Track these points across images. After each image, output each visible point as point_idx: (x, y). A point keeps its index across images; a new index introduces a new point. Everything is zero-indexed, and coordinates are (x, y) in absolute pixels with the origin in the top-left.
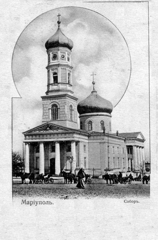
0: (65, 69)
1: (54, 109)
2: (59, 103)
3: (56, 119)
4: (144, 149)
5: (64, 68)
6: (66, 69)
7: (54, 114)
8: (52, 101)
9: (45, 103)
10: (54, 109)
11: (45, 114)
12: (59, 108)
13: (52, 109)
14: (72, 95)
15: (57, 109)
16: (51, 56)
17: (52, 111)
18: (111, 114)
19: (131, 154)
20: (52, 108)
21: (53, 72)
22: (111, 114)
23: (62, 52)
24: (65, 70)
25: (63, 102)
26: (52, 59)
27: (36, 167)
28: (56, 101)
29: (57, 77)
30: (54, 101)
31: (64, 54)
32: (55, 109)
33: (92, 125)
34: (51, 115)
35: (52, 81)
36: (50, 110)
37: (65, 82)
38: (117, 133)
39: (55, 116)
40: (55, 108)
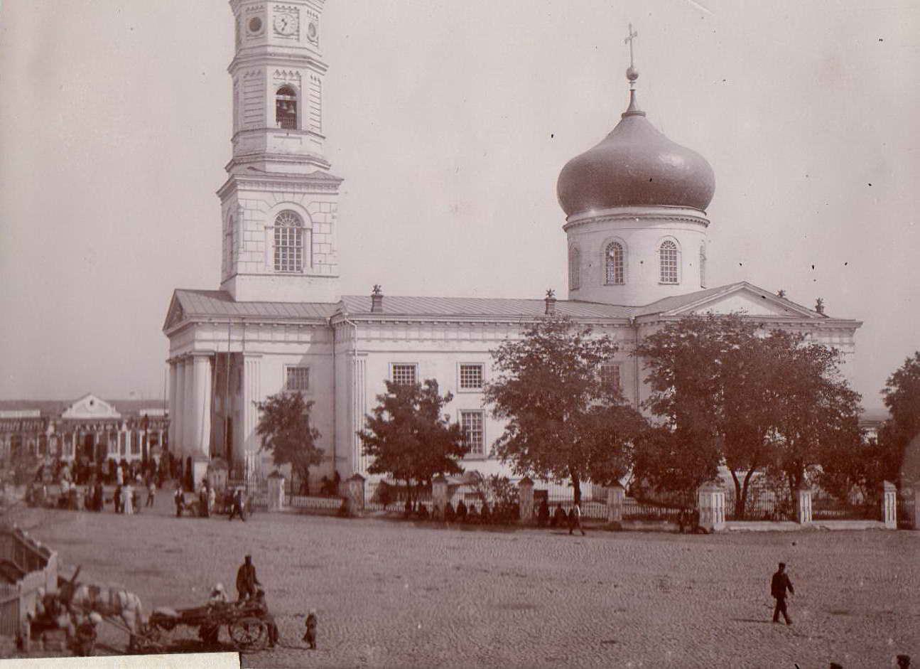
0: (297, 73)
1: (284, 231)
2: (305, 204)
3: (292, 268)
4: (320, 612)
5: (294, 71)
6: (320, 82)
7: (284, 249)
8: (279, 197)
10: (284, 231)
13: (277, 230)
14: (275, 134)
15: (299, 232)
16: (245, 25)
17: (277, 237)
18: (706, 214)
19: (656, 491)
20: (277, 223)
25: (325, 208)
26: (247, 32)
27: (7, 489)
28: (297, 198)
30: (288, 197)
32: (291, 231)
33: (232, 238)
36: (272, 233)
38: (377, 297)
39: (292, 256)
40: (288, 226)
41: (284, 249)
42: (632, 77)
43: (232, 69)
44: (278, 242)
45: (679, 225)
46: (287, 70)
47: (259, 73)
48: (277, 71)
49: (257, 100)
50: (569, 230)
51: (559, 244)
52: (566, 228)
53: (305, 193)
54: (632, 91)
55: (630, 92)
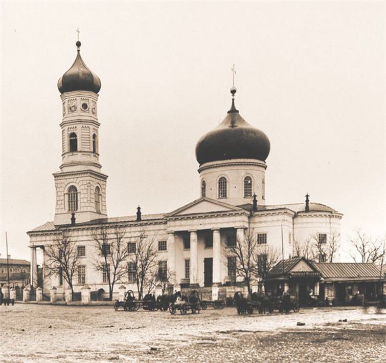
0: (88, 127)
5: (87, 126)
7: (72, 202)
9: (59, 185)
10: (72, 194)
11: (59, 203)
12: (80, 193)
13: (69, 195)
15: (77, 194)
18: (265, 163)
21: (69, 132)
22: (266, 161)
23: (83, 98)
24: (88, 129)
29: (76, 140)
30: (72, 180)
31: (87, 103)
32: (74, 194)
34: (67, 204)
35: (67, 149)
37: (88, 150)
41: (72, 202)
42: (233, 92)
43: (228, 112)
44: (69, 200)
45: (252, 167)
46: (87, 126)
47: (76, 127)
48: (83, 127)
49: (83, 136)
50: (202, 173)
51: (197, 178)
52: (200, 171)
53: (77, 178)
54: (233, 100)
55: (77, 52)
